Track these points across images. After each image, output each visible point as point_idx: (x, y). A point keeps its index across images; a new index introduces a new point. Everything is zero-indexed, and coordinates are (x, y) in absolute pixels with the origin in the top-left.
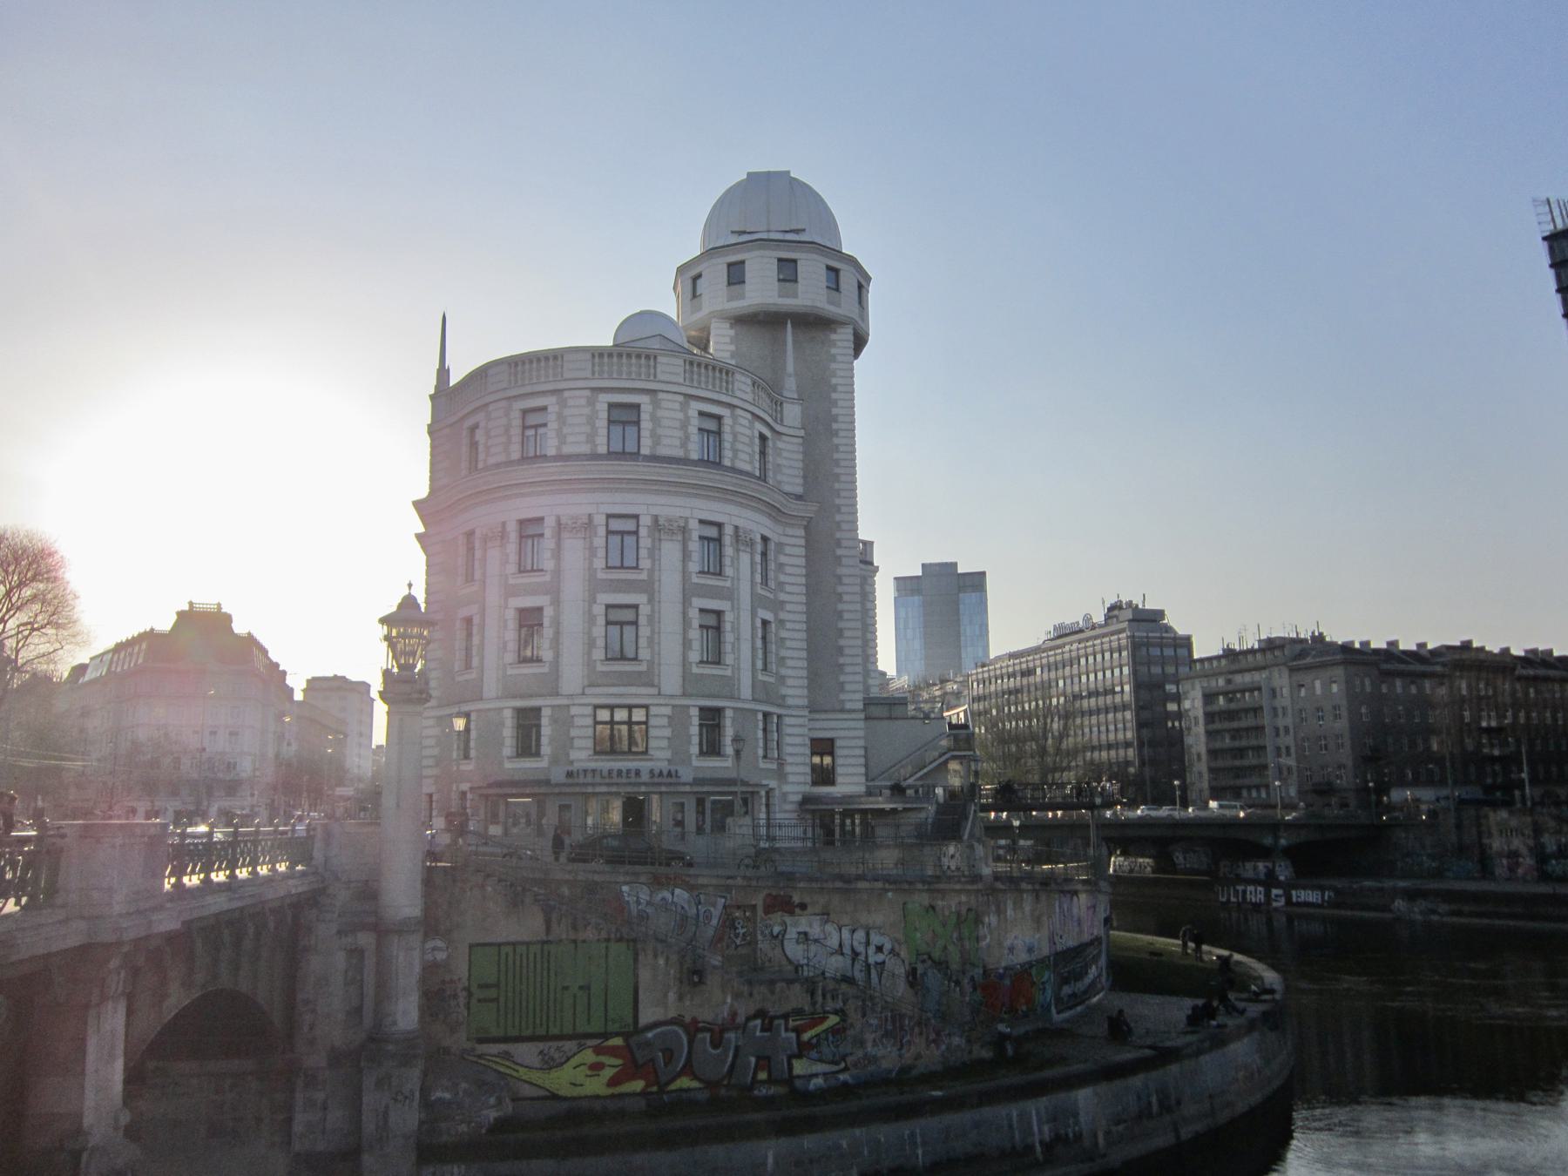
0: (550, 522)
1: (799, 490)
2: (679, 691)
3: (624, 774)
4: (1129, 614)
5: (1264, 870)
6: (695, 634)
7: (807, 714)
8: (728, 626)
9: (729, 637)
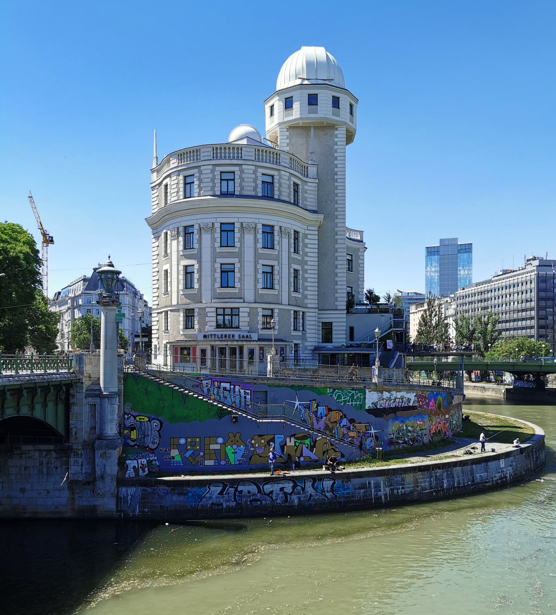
0: (196, 227)
1: (315, 209)
2: (253, 301)
3: (228, 336)
4: (536, 263)
5: (145, 462)
6: (260, 276)
7: (317, 311)
8: (276, 272)
9: (276, 277)
